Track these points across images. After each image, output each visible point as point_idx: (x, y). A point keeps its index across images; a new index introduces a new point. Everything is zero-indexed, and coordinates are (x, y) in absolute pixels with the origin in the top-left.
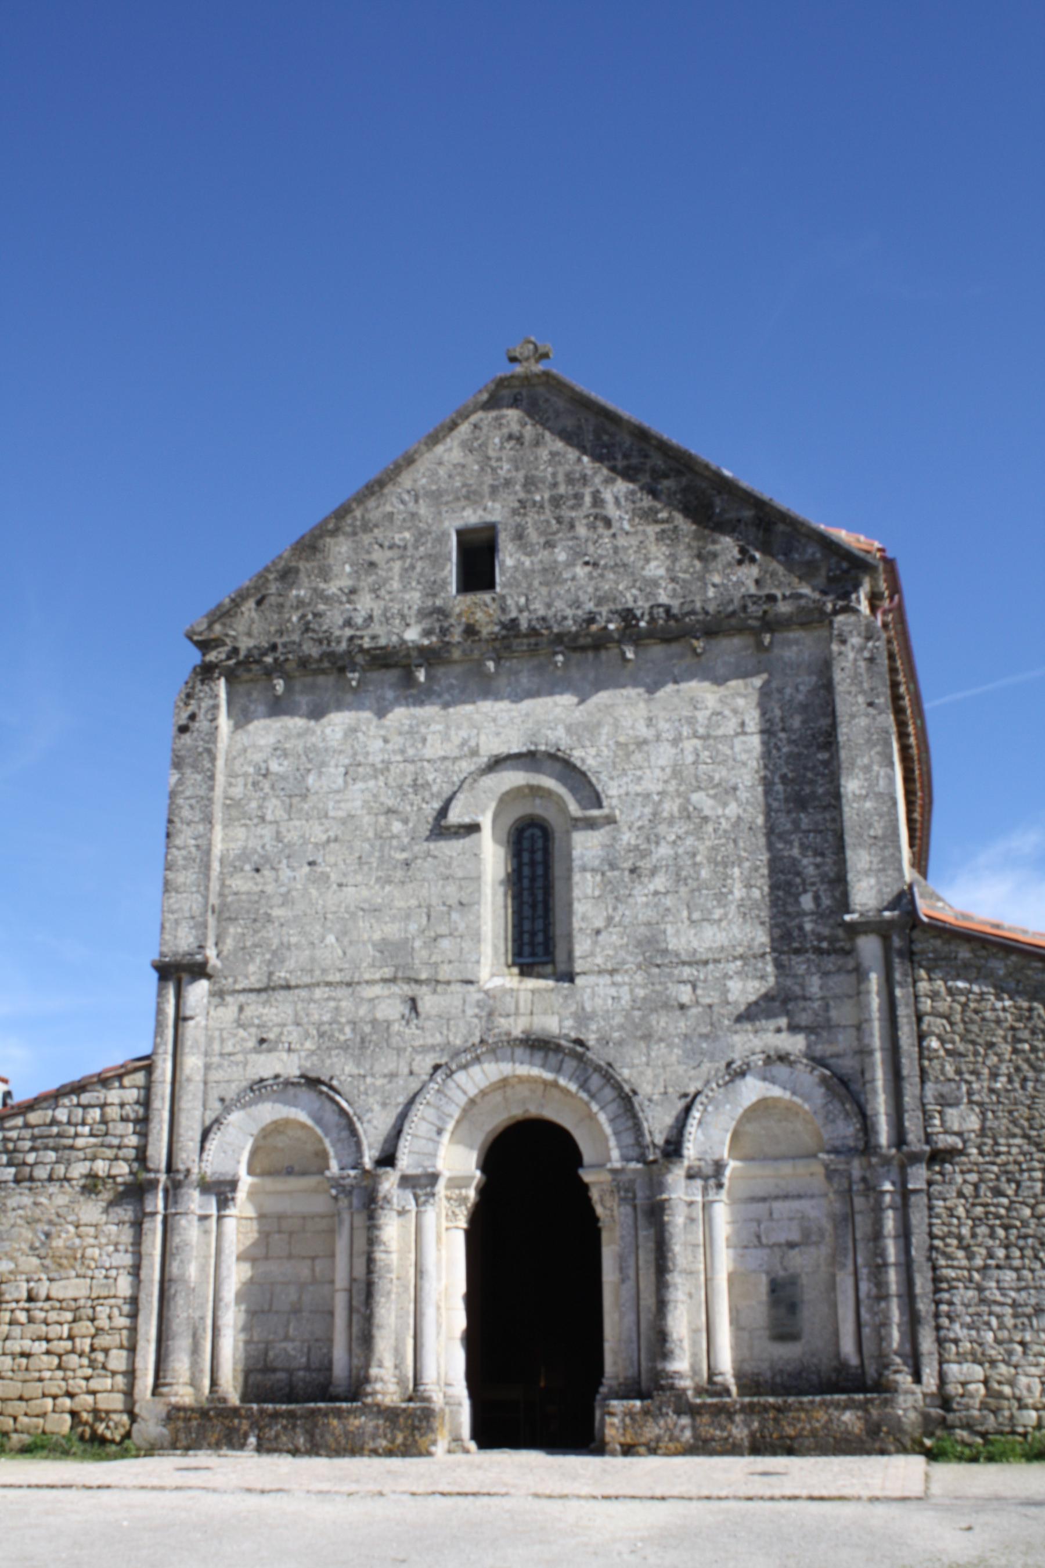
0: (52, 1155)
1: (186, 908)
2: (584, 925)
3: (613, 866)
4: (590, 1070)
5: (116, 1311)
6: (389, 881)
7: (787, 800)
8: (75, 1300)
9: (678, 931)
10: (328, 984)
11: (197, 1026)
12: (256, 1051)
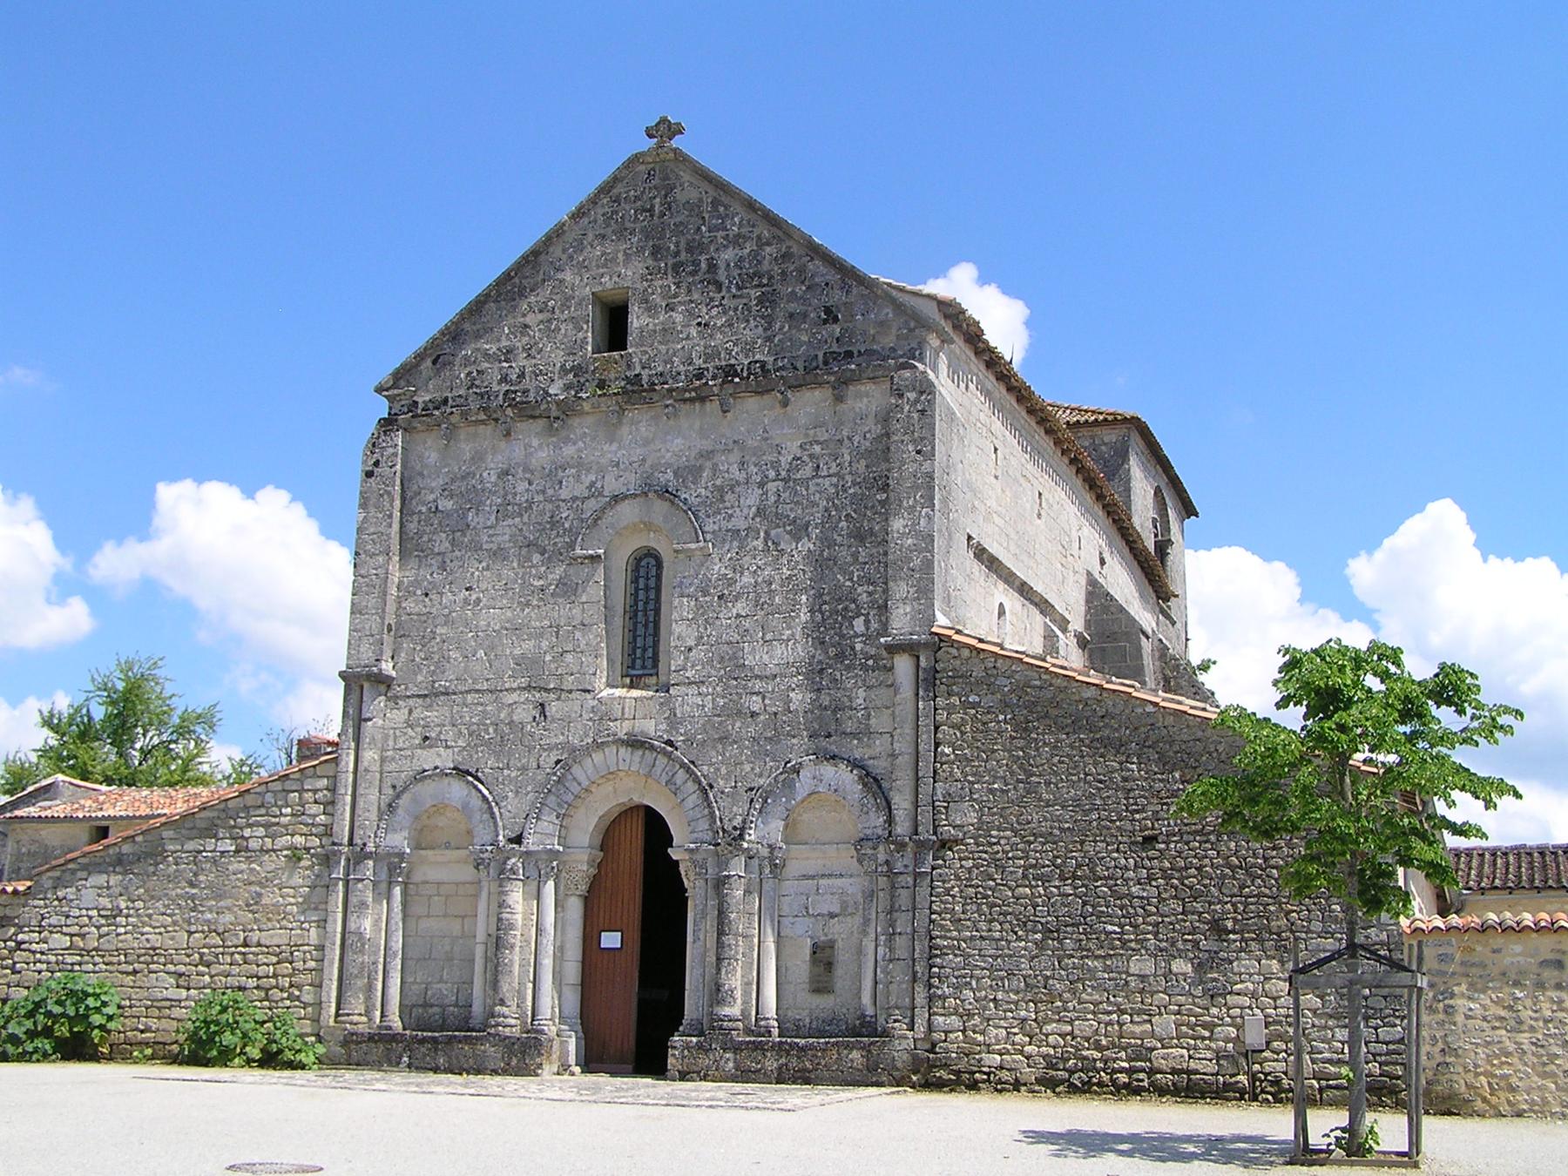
0: (261, 831)
1: (367, 627)
2: (679, 644)
3: (705, 593)
4: (678, 767)
5: (309, 956)
6: (528, 604)
7: (849, 536)
8: (278, 946)
9: (754, 649)
10: (477, 691)
11: (374, 726)
12: (421, 747)
